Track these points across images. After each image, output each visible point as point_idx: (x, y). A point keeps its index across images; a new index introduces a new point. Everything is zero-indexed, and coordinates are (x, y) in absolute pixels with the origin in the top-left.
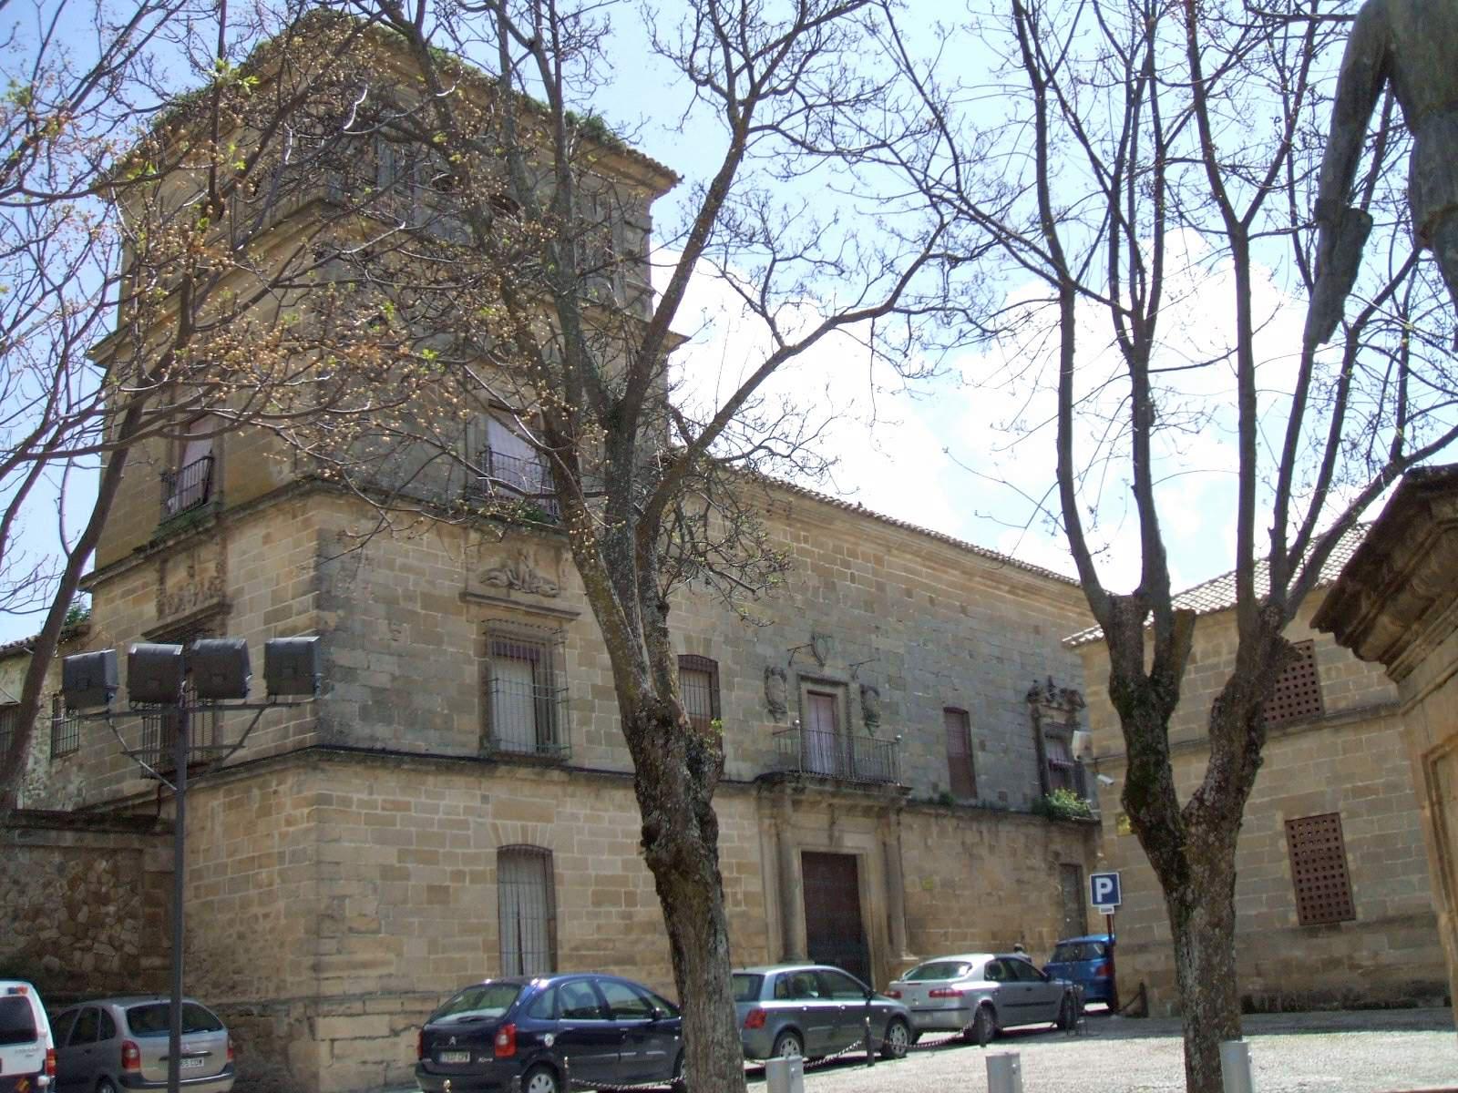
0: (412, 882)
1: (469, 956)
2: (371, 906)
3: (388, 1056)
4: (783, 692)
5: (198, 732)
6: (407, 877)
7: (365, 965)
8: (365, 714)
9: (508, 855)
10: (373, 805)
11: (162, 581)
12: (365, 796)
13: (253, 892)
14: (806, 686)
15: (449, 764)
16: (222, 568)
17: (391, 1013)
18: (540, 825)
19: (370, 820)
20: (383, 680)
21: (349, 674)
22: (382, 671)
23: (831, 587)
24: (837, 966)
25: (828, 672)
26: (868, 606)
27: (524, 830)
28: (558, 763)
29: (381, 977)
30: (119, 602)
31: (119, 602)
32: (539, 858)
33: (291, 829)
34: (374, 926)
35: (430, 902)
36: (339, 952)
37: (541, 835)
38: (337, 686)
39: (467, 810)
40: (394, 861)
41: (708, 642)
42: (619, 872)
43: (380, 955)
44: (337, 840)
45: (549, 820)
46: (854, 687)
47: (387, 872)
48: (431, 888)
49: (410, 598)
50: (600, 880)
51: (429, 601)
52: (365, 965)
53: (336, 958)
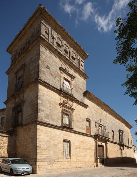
0: (51, 143)
1: (59, 154)
2: (45, 146)
3: (47, 168)
4: (97, 125)
5: (19, 121)
6: (51, 142)
7: (44, 154)
8: (45, 117)
9: (65, 141)
10: (46, 131)
11: (15, 101)
12: (45, 129)
13: (27, 143)
14: (99, 125)
15: (57, 127)
16: (23, 97)
17: (48, 162)
18: (69, 137)
19: (45, 133)
20: (48, 113)
21: (43, 111)
22: (48, 112)
23: (102, 113)
24: (20, 158)
25: (101, 124)
26: (105, 117)
27: (67, 137)
28: (71, 129)
29: (46, 156)
30: (9, 105)
31: (9, 105)
32: (69, 142)
33: (33, 134)
34: (46, 149)
35: (54, 146)
36: (40, 152)
37: (69, 139)
38: (41, 112)
39: (60, 134)
40: (49, 140)
41: (89, 117)
42: (78, 145)
43: (46, 153)
44: (41, 135)
45: (70, 137)
46: (104, 126)
47: (47, 141)
48: (54, 144)
49: (52, 102)
50: (76, 145)
51: (55, 103)
52: (44, 154)
53: (40, 153)
